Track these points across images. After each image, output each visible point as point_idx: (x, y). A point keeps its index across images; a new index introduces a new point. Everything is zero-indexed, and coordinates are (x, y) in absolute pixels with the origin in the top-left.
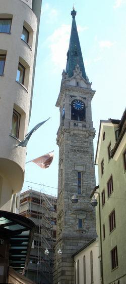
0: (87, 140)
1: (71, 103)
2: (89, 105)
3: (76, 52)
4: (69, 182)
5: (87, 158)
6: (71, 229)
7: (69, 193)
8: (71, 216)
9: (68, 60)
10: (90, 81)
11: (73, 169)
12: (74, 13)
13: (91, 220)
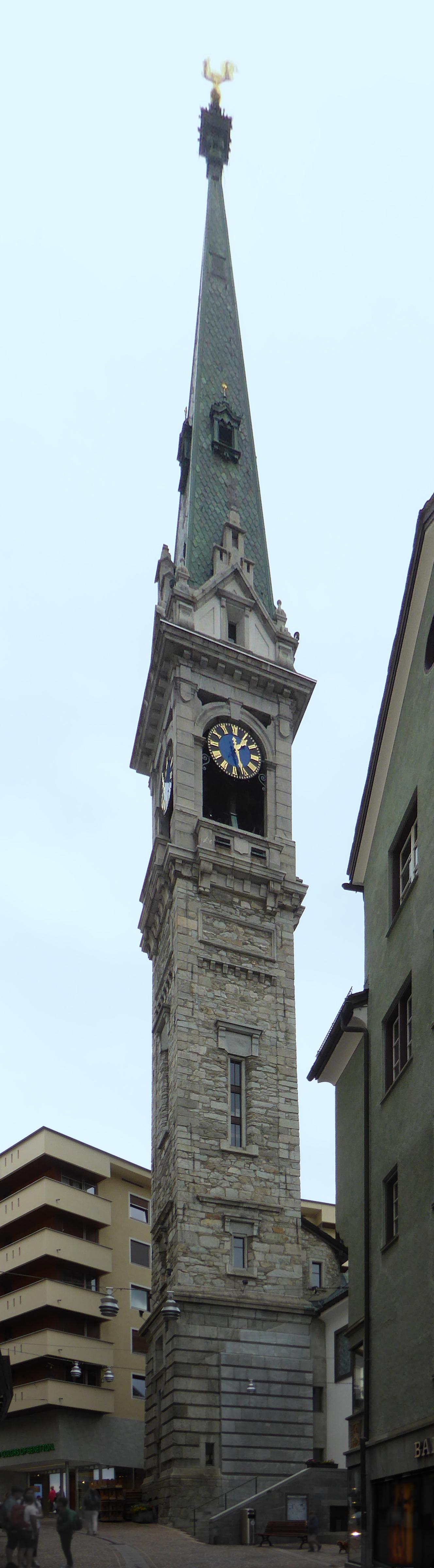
0: (269, 925)
1: (200, 733)
2: (280, 760)
3: (226, 434)
4: (194, 1097)
5: (268, 1006)
6: (206, 1269)
7: (195, 1137)
8: (208, 1222)
9: (182, 488)
10: (291, 627)
11: (211, 1043)
12: (215, 134)
13: (278, 1243)
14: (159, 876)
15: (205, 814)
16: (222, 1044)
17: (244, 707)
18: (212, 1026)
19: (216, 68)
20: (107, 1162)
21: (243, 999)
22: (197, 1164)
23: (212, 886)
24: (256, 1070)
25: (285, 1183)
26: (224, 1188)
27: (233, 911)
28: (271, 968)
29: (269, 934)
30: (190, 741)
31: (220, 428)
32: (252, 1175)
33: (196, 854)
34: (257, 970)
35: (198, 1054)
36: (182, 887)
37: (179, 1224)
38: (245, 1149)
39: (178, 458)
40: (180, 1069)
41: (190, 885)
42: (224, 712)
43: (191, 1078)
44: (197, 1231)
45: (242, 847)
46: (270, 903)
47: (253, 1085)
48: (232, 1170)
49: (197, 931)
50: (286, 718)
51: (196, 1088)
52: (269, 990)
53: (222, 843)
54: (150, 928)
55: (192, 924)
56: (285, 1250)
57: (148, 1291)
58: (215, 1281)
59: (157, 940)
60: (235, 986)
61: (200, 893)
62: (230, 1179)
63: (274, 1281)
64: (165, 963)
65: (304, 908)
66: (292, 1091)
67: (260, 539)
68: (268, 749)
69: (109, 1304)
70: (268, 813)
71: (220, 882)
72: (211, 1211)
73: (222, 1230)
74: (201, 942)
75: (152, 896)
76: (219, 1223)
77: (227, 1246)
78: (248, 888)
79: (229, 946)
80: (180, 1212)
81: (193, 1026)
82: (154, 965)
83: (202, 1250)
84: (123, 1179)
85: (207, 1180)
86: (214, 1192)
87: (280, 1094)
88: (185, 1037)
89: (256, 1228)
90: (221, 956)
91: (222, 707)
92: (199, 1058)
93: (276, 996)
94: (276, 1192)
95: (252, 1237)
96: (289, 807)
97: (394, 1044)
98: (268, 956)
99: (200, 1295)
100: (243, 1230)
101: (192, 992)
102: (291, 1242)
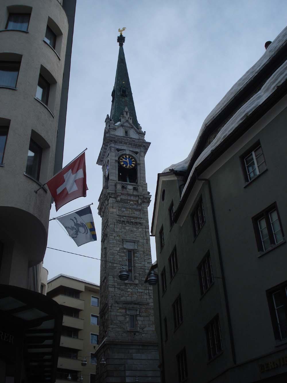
0: (140, 207)
1: (117, 159)
2: (141, 162)
3: (124, 92)
4: (115, 265)
6: (119, 330)
8: (120, 310)
9: (113, 101)
10: (143, 130)
11: (121, 246)
12: (121, 40)
13: (147, 316)
14: (104, 197)
15: (119, 180)
16: (125, 246)
17: (130, 151)
18: (121, 241)
19: (121, 29)
20: (84, 285)
21: (132, 231)
22: (116, 289)
23: (121, 199)
24: (137, 253)
25: (149, 293)
26: (126, 297)
27: (128, 205)
28: (141, 220)
29: (140, 210)
30: (114, 161)
31: (123, 91)
32: (136, 291)
33: (116, 191)
34: (136, 221)
35: (117, 250)
36: (111, 200)
37: (109, 312)
38: (133, 282)
39: (112, 96)
40: (110, 256)
41: (114, 199)
42: (124, 153)
43: (114, 259)
44: (117, 314)
45: (130, 187)
46: (140, 201)
47: (136, 259)
48: (129, 290)
49: (116, 212)
50: (142, 152)
51: (116, 262)
52: (140, 227)
53: (123, 187)
54: (101, 209)
55: (114, 210)
56: (150, 319)
57: (97, 335)
58: (123, 334)
59: (104, 212)
60: (129, 227)
61: (117, 201)
62: (128, 293)
63: (146, 332)
64: (106, 220)
65: (151, 195)
66: (150, 259)
67: (134, 111)
68: (138, 160)
69: (84, 362)
70: (138, 176)
71: (123, 197)
72: (121, 306)
73: (125, 313)
74: (117, 215)
75: (102, 201)
76: (124, 311)
77: (128, 319)
78: (132, 198)
79: (127, 215)
80: (110, 308)
81: (115, 241)
82: (102, 219)
83: (118, 322)
84: (90, 291)
85: (120, 294)
86: (123, 299)
87: (145, 261)
88: (112, 245)
89: (138, 311)
90: (124, 218)
91: (124, 152)
92: (117, 251)
93: (143, 229)
94: (145, 297)
95: (137, 315)
96: (145, 174)
97: (199, 216)
98: (139, 217)
99: (117, 341)
100: (133, 313)
101: (115, 231)
102: (152, 316)
